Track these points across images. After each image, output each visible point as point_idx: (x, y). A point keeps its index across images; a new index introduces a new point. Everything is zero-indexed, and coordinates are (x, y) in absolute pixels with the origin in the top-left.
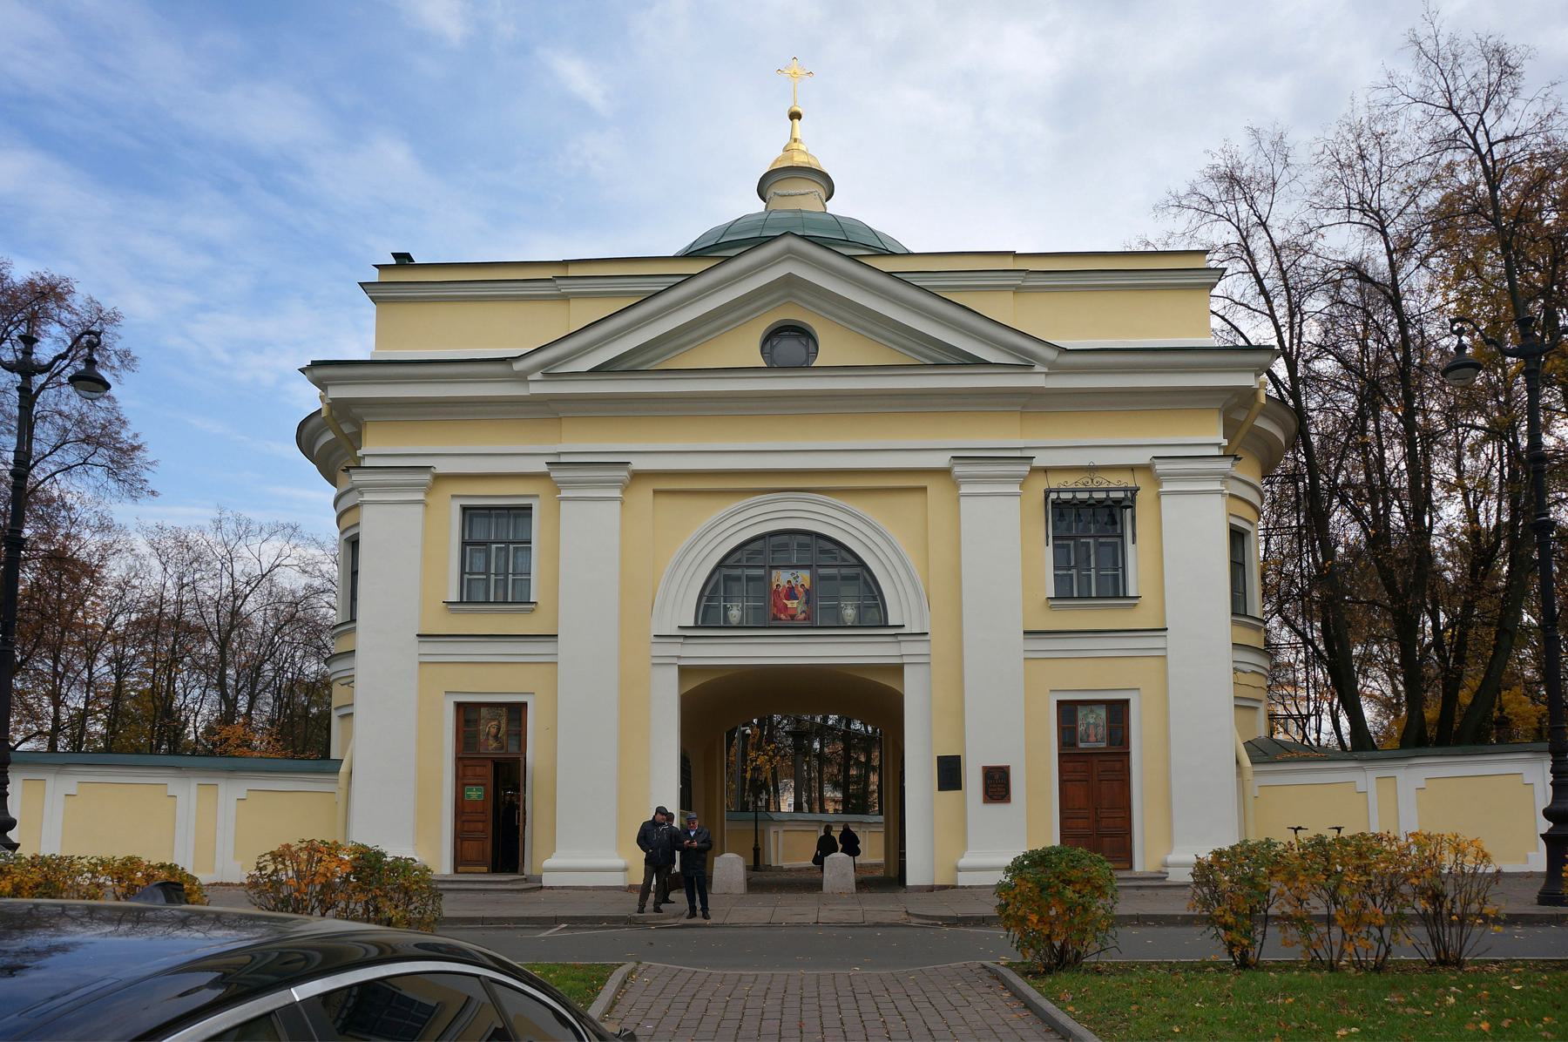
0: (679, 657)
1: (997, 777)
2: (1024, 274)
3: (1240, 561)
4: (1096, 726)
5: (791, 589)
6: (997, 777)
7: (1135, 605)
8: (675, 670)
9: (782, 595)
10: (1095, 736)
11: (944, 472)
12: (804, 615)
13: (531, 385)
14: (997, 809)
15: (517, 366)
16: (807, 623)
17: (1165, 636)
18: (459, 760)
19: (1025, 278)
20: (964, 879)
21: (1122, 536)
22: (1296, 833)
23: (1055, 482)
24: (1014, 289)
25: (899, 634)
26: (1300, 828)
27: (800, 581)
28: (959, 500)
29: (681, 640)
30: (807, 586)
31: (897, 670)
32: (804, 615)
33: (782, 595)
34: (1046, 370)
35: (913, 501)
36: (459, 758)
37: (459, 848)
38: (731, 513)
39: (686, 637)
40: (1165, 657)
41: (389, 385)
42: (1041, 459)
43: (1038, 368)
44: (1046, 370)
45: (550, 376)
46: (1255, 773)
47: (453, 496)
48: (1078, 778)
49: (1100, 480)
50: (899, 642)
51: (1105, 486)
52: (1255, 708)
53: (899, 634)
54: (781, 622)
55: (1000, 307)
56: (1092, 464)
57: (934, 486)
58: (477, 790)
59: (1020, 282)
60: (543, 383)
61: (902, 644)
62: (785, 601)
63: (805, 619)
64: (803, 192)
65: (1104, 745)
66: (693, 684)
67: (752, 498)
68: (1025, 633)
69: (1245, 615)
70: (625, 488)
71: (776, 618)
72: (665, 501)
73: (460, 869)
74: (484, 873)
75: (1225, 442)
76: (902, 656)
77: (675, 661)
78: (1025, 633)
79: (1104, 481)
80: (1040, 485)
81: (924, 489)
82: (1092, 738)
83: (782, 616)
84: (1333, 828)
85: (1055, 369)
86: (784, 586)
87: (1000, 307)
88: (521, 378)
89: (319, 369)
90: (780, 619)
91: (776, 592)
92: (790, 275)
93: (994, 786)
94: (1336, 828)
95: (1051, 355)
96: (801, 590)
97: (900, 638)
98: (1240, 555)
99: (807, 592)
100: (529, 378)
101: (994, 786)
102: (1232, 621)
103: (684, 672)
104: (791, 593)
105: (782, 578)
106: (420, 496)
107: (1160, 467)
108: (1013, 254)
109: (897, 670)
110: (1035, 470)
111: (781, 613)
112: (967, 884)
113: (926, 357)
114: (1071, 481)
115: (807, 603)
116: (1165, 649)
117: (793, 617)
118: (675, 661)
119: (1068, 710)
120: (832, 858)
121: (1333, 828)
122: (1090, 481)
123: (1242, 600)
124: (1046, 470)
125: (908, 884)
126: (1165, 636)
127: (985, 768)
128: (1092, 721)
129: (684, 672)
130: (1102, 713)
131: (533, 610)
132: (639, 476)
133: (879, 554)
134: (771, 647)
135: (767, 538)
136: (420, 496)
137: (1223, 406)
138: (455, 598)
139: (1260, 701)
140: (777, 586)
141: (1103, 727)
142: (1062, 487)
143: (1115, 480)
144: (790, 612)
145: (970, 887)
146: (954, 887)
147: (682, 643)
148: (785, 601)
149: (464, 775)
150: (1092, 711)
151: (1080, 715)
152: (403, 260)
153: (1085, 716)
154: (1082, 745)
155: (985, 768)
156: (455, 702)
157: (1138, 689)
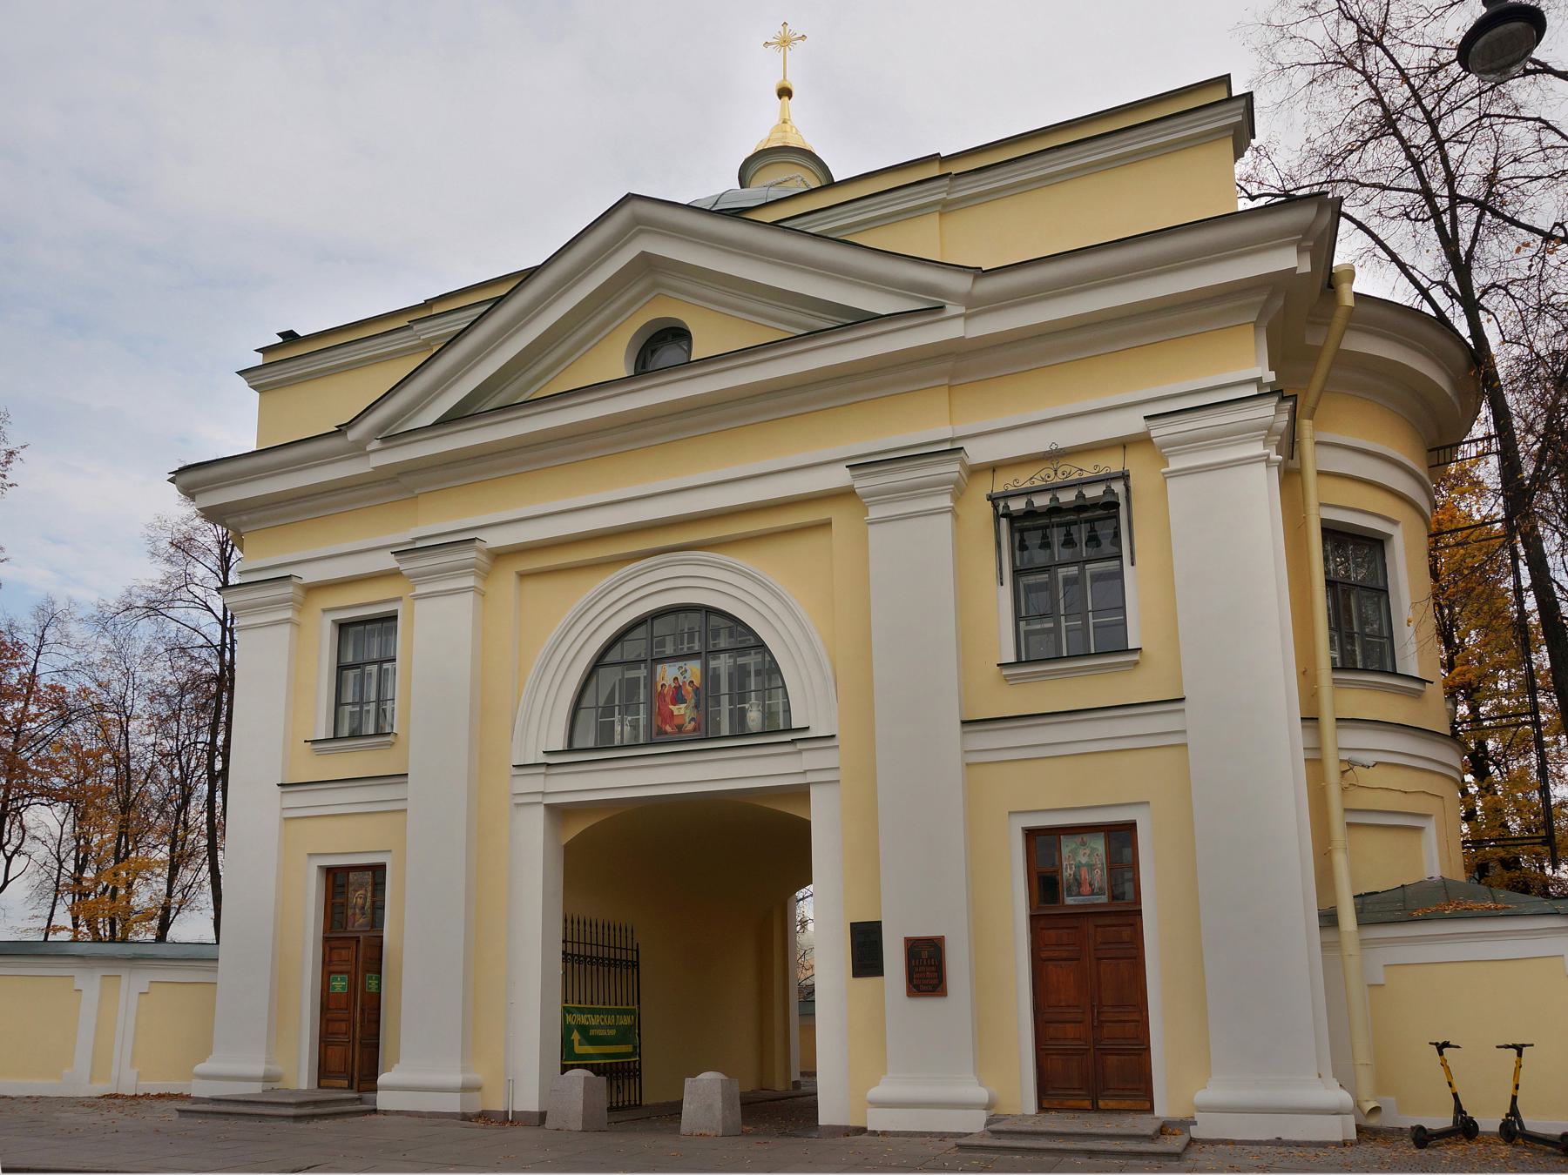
0: (543, 793)
1: (925, 955)
2: (946, 181)
3: (1381, 584)
4: (1091, 867)
5: (678, 689)
6: (925, 955)
7: (1136, 663)
8: (540, 812)
9: (668, 699)
10: (1091, 885)
11: (844, 495)
12: (693, 723)
13: (372, 456)
14: (927, 1006)
15: (353, 435)
16: (696, 735)
17: (1183, 710)
18: (1034, 919)
19: (950, 188)
20: (877, 1120)
21: (1119, 557)
22: (1441, 1054)
23: (1003, 483)
24: (939, 208)
25: (800, 738)
26: (1446, 1045)
27: (689, 678)
28: (865, 537)
29: (543, 770)
30: (697, 683)
31: (801, 793)
32: (693, 723)
33: (668, 699)
34: (962, 310)
35: (815, 541)
36: (326, 938)
37: (323, 1056)
38: (601, 592)
39: (548, 765)
40: (1186, 745)
41: (248, 484)
42: (979, 452)
43: (952, 309)
44: (962, 310)
45: (390, 437)
46: (1363, 943)
47: (325, 611)
48: (1065, 955)
49: (1067, 469)
50: (800, 752)
51: (1076, 476)
52: (1419, 829)
53: (800, 738)
54: (667, 736)
55: (921, 238)
56: (1054, 447)
57: (839, 515)
58: (342, 980)
59: (944, 195)
60: (382, 453)
61: (805, 754)
62: (671, 707)
63: (695, 730)
64: (779, 180)
65: (1104, 899)
66: (575, 829)
67: (628, 567)
68: (964, 723)
69: (1394, 674)
70: (485, 574)
71: (661, 732)
72: (535, 588)
73: (323, 1082)
74: (345, 1088)
75: (1270, 377)
76: (805, 772)
77: (538, 798)
78: (964, 723)
79: (1074, 470)
80: (985, 486)
81: (826, 525)
82: (1086, 889)
83: (668, 728)
84: (1508, 1047)
85: (977, 306)
86: (670, 685)
87: (921, 238)
88: (359, 450)
89: (190, 479)
90: (666, 733)
91: (661, 695)
92: (644, 256)
93: (921, 969)
94: (1514, 1046)
95: (962, 283)
96: (690, 689)
97: (800, 746)
98: (1380, 576)
99: (696, 690)
100: (368, 449)
101: (921, 969)
102: (1335, 681)
103: (559, 813)
104: (678, 697)
105: (667, 674)
106: (288, 614)
107: (1160, 431)
108: (935, 158)
109: (801, 793)
110: (975, 471)
111: (666, 723)
112: (879, 1129)
113: (798, 325)
114: (1023, 479)
115: (697, 706)
116: (1184, 732)
117: (680, 728)
118: (538, 798)
119: (1041, 842)
120: (701, 1080)
121: (1508, 1047)
122: (1052, 473)
123: (1387, 648)
124: (994, 468)
125: (821, 1122)
126: (1183, 710)
127: (907, 940)
128: (1084, 860)
129: (559, 813)
130: (1098, 845)
131: (393, 744)
132: (500, 555)
133: (777, 625)
134: (645, 772)
135: (649, 621)
136: (288, 614)
137: (1260, 316)
138: (560, 745)
139: (1426, 816)
140: (662, 686)
141: (1102, 870)
142: (1011, 488)
143: (1089, 467)
144: (677, 721)
145: (884, 1133)
146: (862, 1130)
147: (546, 775)
148: (671, 707)
149: (330, 961)
150: (1083, 844)
151: (1065, 851)
152: (290, 337)
153: (1074, 852)
154: (1069, 901)
155: (907, 940)
156: (320, 867)
157: (838, 768)
